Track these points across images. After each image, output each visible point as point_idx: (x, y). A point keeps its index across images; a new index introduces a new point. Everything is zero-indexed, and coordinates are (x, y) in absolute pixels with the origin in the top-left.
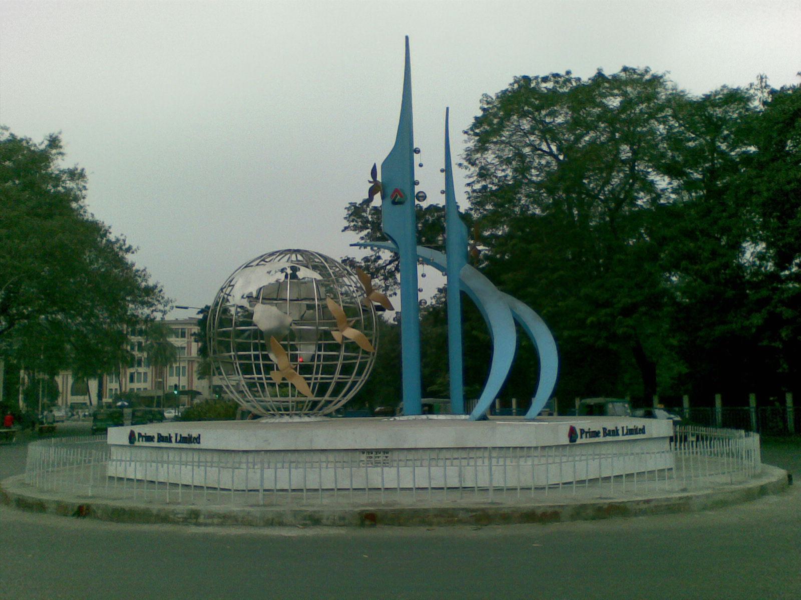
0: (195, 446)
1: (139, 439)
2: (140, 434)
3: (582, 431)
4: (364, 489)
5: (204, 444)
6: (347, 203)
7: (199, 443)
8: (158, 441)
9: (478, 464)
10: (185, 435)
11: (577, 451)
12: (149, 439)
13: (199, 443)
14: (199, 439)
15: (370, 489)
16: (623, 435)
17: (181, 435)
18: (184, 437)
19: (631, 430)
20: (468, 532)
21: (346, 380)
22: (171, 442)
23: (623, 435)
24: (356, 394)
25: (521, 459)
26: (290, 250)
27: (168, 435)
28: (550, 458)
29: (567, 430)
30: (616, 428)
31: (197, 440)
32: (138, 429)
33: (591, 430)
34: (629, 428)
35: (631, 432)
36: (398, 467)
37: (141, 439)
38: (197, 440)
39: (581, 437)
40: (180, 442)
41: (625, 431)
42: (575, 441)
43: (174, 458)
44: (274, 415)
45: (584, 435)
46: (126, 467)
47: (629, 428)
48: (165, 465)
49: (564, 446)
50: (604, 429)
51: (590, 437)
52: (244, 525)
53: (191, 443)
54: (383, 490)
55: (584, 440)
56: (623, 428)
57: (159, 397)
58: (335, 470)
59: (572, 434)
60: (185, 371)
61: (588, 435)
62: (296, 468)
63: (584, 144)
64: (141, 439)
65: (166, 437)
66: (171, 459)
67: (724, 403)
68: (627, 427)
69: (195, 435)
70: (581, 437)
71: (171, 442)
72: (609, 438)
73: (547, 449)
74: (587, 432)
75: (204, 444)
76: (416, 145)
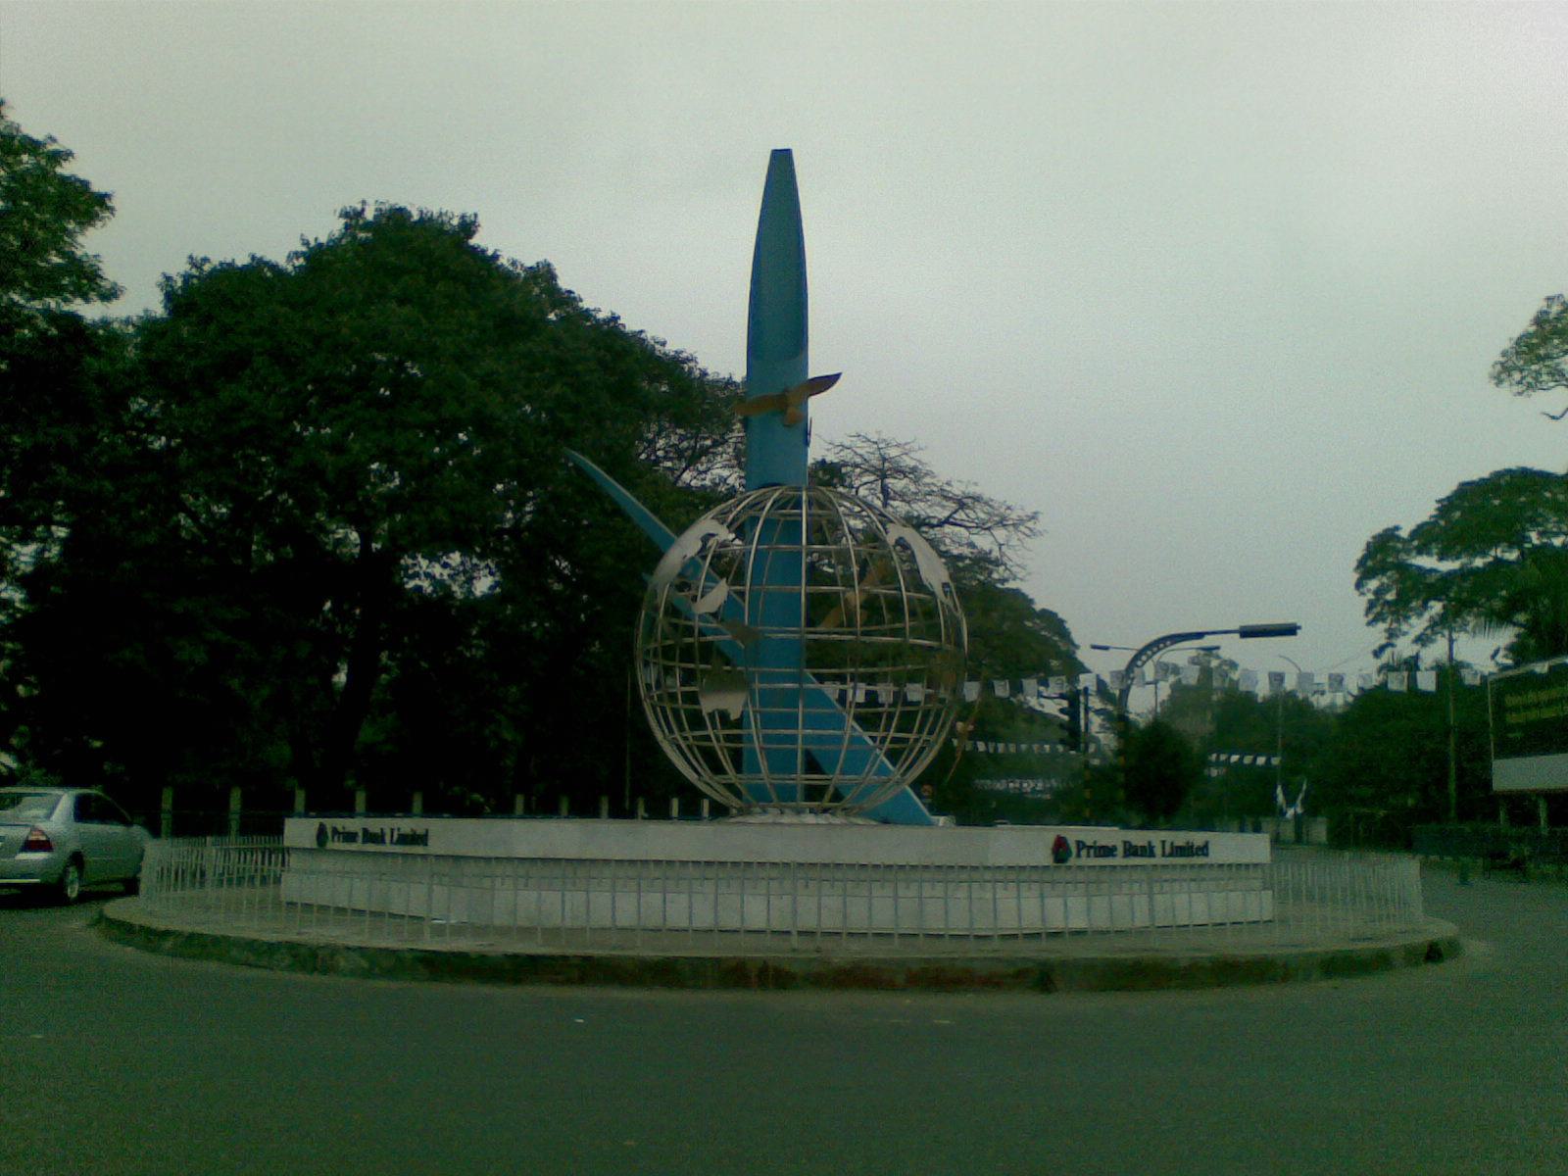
0: (419, 850)
1: (333, 838)
2: (335, 831)
3: (1080, 845)
4: (403, 916)
7: (1207, 855)
8: (364, 842)
9: (924, 895)
11: (326, 863)
12: (350, 837)
13: (1207, 855)
14: (1207, 849)
16: (1164, 855)
17: (1172, 843)
18: (1178, 847)
19: (1180, 848)
22: (383, 841)
23: (1164, 855)
24: (923, 772)
25: (681, 882)
27: (379, 831)
28: (556, 880)
29: (314, 831)
30: (1150, 843)
31: (1204, 850)
32: (1074, 834)
33: (1098, 844)
34: (402, 831)
36: (664, 892)
37: (336, 838)
38: (1204, 850)
39: (1079, 855)
40: (1171, 855)
45: (1084, 852)
49: (311, 850)
50: (365, 831)
51: (1096, 856)
52: (573, 983)
53: (1193, 855)
54: (844, 936)
55: (1084, 861)
56: (1163, 842)
58: (690, 897)
60: (891, 725)
61: (1092, 851)
62: (440, 884)
63: (652, 390)
64: (336, 838)
65: (1143, 847)
67: (246, 802)
68: (399, 829)
69: (420, 831)
71: (1152, 855)
72: (371, 847)
73: (716, 867)
74: (1091, 847)
75: (435, 846)
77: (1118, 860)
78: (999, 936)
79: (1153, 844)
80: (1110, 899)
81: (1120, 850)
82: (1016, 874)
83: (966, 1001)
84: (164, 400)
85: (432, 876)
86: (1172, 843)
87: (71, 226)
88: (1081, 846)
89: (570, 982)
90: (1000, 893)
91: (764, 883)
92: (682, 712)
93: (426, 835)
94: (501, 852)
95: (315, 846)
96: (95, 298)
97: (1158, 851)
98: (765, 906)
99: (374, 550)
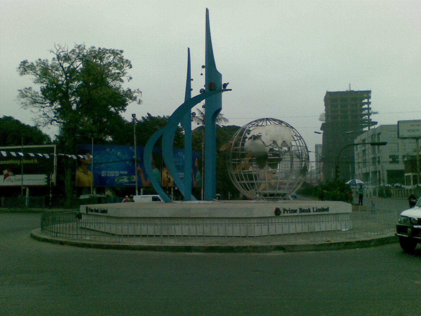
3: (285, 210)
5: (331, 211)
6: (145, 115)
10: (320, 208)
14: (328, 209)
15: (170, 236)
16: (314, 211)
20: (169, 254)
21: (243, 185)
22: (309, 211)
26: (264, 119)
30: (309, 208)
35: (319, 210)
39: (284, 213)
40: (316, 211)
41: (315, 210)
42: (279, 214)
43: (105, 221)
44: (259, 199)
46: (73, 225)
47: (317, 208)
48: (72, 223)
56: (313, 208)
57: (139, 194)
59: (277, 212)
60: (240, 177)
65: (306, 210)
66: (330, 219)
70: (284, 213)
74: (287, 211)
75: (331, 211)
76: (192, 88)
77: (298, 213)
78: (227, 236)
79: (310, 209)
80: (261, 227)
81: (298, 211)
82: (263, 219)
83: (90, 250)
84: (102, 118)
85: (47, 226)
86: (316, 208)
87: (84, 84)
88: (285, 210)
89: (163, 251)
90: (142, 227)
91: (325, 222)
92: (247, 174)
93: (328, 208)
94: (252, 216)
95: (274, 215)
96: (28, 116)
97: (312, 210)
98: (270, 230)
99: (38, 162)
